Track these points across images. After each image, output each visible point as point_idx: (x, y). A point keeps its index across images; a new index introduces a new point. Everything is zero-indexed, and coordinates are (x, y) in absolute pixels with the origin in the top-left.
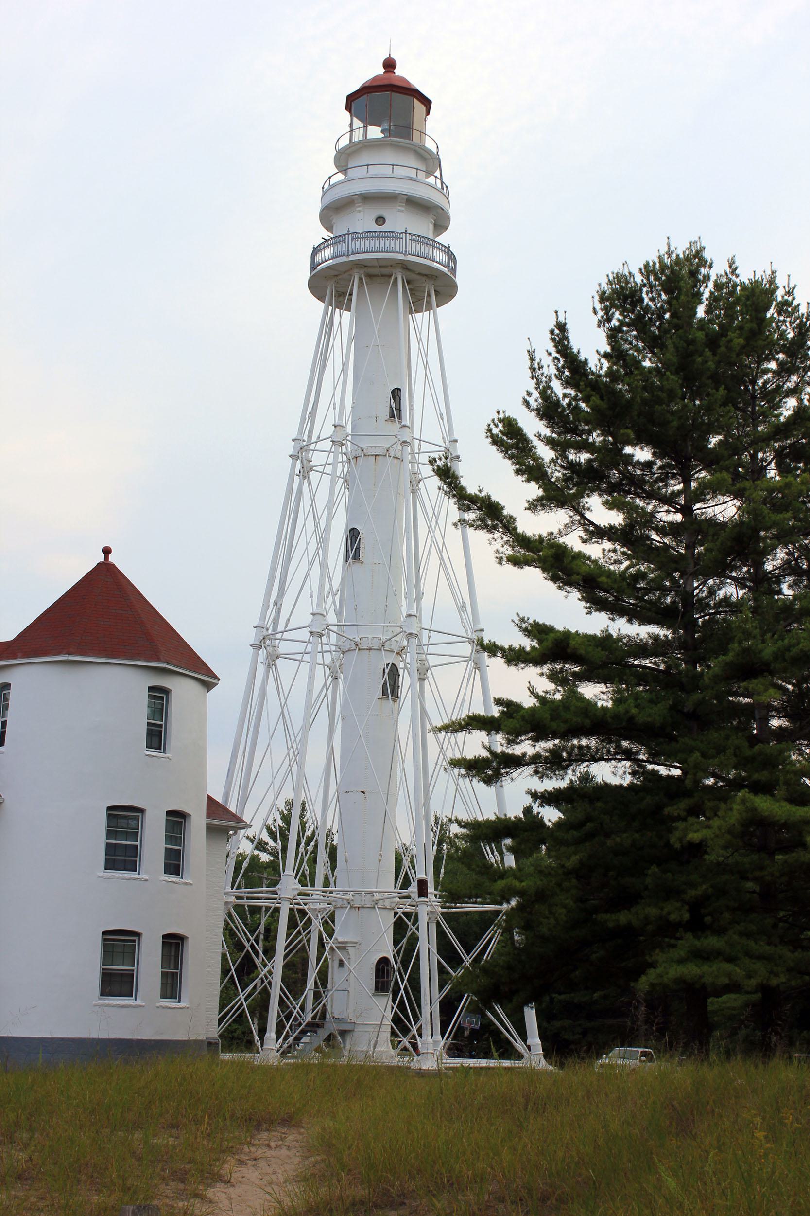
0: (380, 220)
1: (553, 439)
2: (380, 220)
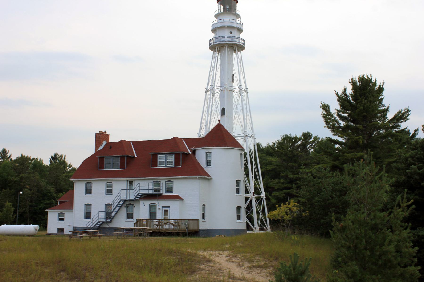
0: (231, 33)
1: (376, 86)
2: (231, 33)
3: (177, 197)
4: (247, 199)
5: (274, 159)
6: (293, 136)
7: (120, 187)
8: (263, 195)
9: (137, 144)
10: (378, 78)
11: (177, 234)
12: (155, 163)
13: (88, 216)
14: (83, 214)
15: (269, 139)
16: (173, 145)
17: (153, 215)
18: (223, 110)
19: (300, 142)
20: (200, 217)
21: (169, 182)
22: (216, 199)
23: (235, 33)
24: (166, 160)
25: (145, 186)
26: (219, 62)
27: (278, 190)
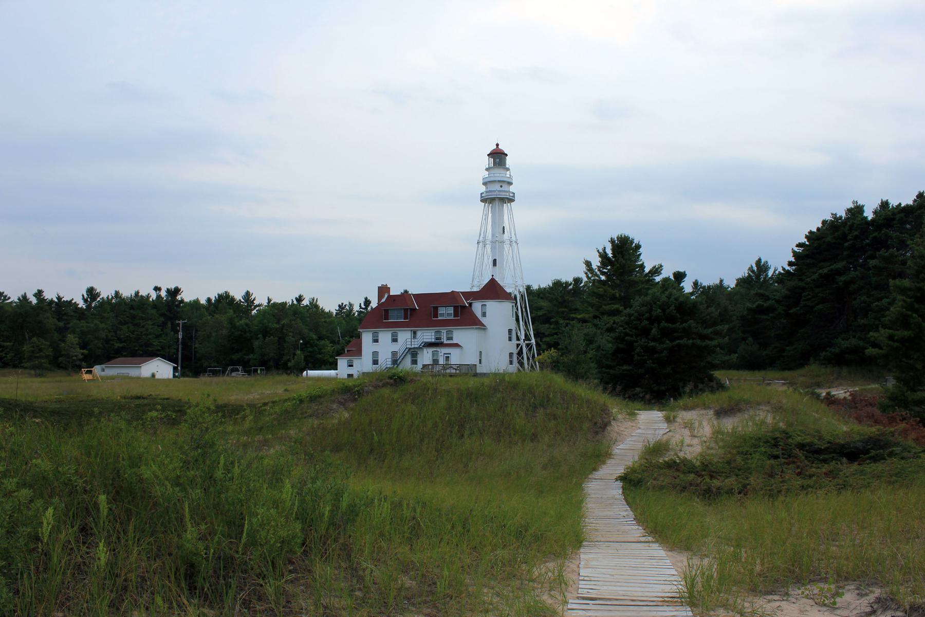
3: (457, 345)
4: (518, 345)
5: (544, 304)
6: (564, 280)
7: (404, 336)
8: (533, 341)
9: (418, 297)
10: (636, 236)
11: (460, 375)
12: (436, 315)
13: (375, 362)
14: (371, 361)
15: (543, 281)
16: (450, 298)
17: (435, 362)
18: (495, 261)
19: (571, 287)
20: (477, 363)
21: (449, 332)
22: (492, 346)
23: (505, 187)
24: (446, 312)
25: (427, 335)
26: (490, 215)
27: (549, 336)
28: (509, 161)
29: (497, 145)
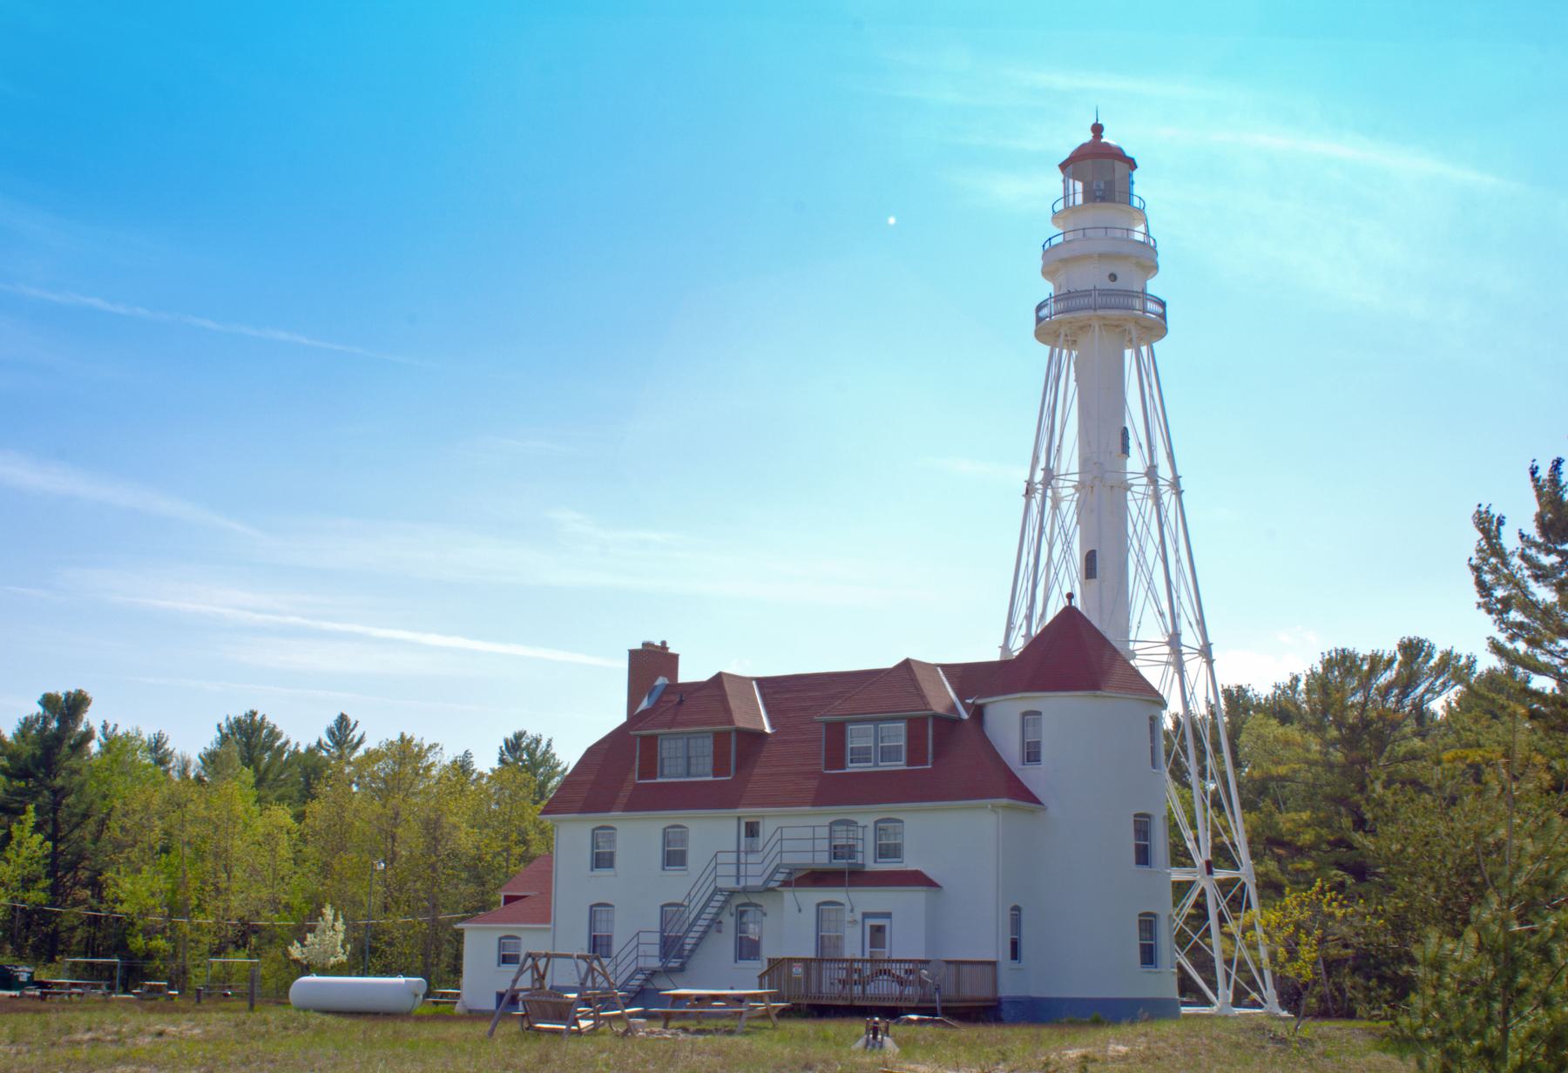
7: (711, 834)
20: (1001, 954)
25: (800, 833)
28: (1143, 186)
29: (1097, 129)
